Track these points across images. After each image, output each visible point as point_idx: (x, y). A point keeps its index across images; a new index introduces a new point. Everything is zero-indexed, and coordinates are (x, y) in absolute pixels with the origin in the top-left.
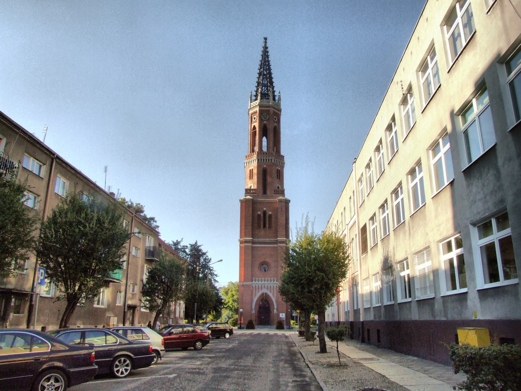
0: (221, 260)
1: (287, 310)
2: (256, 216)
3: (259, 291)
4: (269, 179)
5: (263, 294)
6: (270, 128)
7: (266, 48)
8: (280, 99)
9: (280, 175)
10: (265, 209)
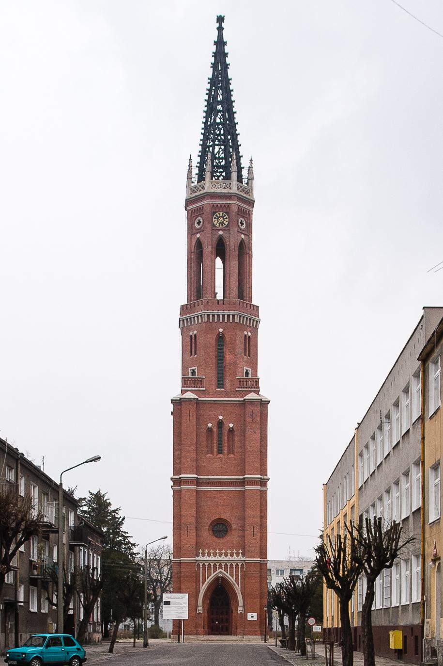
0: (97, 459)
1: (261, 609)
2: (203, 430)
3: (210, 574)
4: (229, 357)
5: (217, 579)
6: (232, 243)
7: (220, 43)
8: (250, 179)
9: (250, 346)
10: (221, 417)
